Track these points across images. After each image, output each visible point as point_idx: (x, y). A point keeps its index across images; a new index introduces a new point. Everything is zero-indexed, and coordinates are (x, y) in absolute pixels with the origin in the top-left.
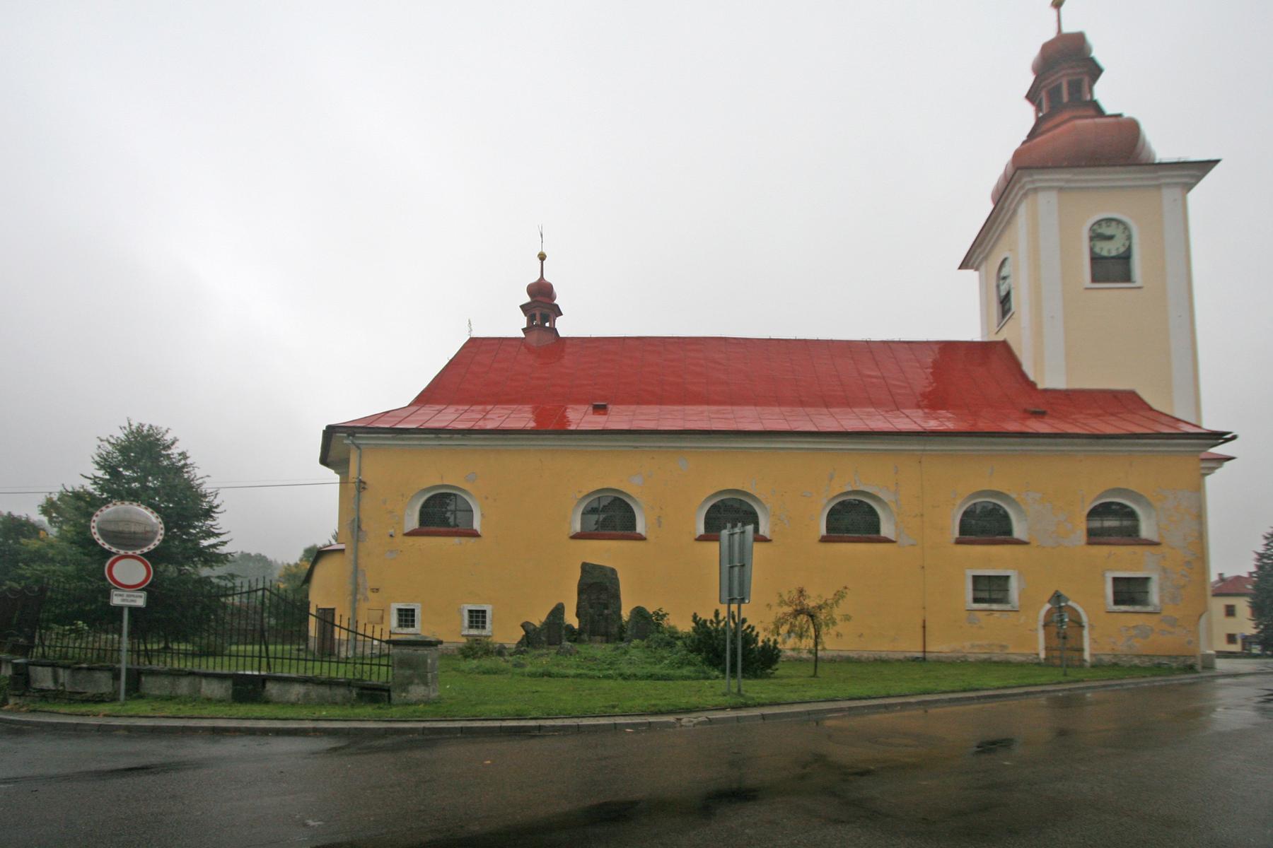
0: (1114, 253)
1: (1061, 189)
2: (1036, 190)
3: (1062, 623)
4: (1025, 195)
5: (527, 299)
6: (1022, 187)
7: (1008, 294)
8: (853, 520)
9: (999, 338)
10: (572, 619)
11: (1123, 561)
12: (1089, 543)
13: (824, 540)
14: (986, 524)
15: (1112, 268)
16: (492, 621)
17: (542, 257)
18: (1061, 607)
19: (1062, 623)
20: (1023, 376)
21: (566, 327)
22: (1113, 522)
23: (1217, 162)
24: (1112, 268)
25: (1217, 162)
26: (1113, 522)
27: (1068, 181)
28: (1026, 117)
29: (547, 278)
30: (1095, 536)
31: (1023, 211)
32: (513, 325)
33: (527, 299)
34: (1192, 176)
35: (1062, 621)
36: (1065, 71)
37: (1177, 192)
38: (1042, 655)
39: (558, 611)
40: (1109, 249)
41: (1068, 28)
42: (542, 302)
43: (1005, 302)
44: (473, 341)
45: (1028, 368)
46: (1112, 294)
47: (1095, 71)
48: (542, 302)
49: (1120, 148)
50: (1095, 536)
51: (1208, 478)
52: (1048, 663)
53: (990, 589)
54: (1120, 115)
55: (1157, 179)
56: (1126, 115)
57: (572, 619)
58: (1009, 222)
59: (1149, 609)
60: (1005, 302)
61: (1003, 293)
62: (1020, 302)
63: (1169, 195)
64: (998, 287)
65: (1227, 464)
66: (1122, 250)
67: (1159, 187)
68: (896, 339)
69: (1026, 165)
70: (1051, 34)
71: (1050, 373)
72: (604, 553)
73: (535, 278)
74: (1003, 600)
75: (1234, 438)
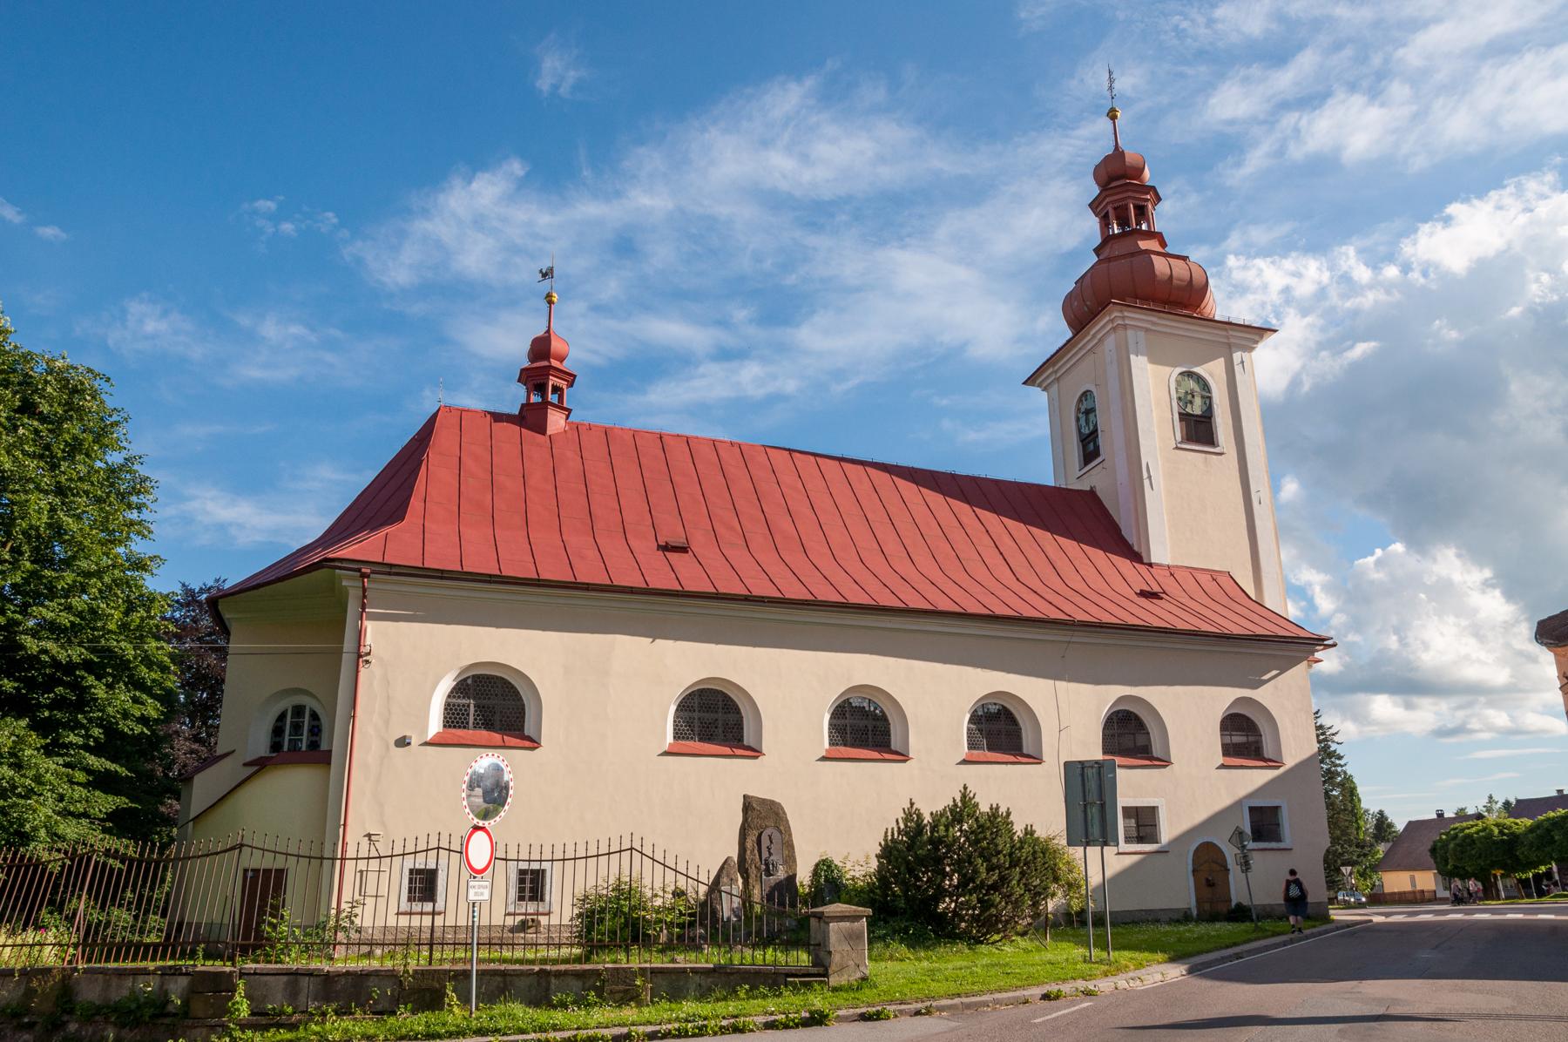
2: (1125, 327)
6: (1112, 321)
22: (1244, 737)
27: (1154, 323)
32: (514, 397)
46: (1194, 459)
59: (1281, 845)
61: (1086, 431)
75: (1334, 645)
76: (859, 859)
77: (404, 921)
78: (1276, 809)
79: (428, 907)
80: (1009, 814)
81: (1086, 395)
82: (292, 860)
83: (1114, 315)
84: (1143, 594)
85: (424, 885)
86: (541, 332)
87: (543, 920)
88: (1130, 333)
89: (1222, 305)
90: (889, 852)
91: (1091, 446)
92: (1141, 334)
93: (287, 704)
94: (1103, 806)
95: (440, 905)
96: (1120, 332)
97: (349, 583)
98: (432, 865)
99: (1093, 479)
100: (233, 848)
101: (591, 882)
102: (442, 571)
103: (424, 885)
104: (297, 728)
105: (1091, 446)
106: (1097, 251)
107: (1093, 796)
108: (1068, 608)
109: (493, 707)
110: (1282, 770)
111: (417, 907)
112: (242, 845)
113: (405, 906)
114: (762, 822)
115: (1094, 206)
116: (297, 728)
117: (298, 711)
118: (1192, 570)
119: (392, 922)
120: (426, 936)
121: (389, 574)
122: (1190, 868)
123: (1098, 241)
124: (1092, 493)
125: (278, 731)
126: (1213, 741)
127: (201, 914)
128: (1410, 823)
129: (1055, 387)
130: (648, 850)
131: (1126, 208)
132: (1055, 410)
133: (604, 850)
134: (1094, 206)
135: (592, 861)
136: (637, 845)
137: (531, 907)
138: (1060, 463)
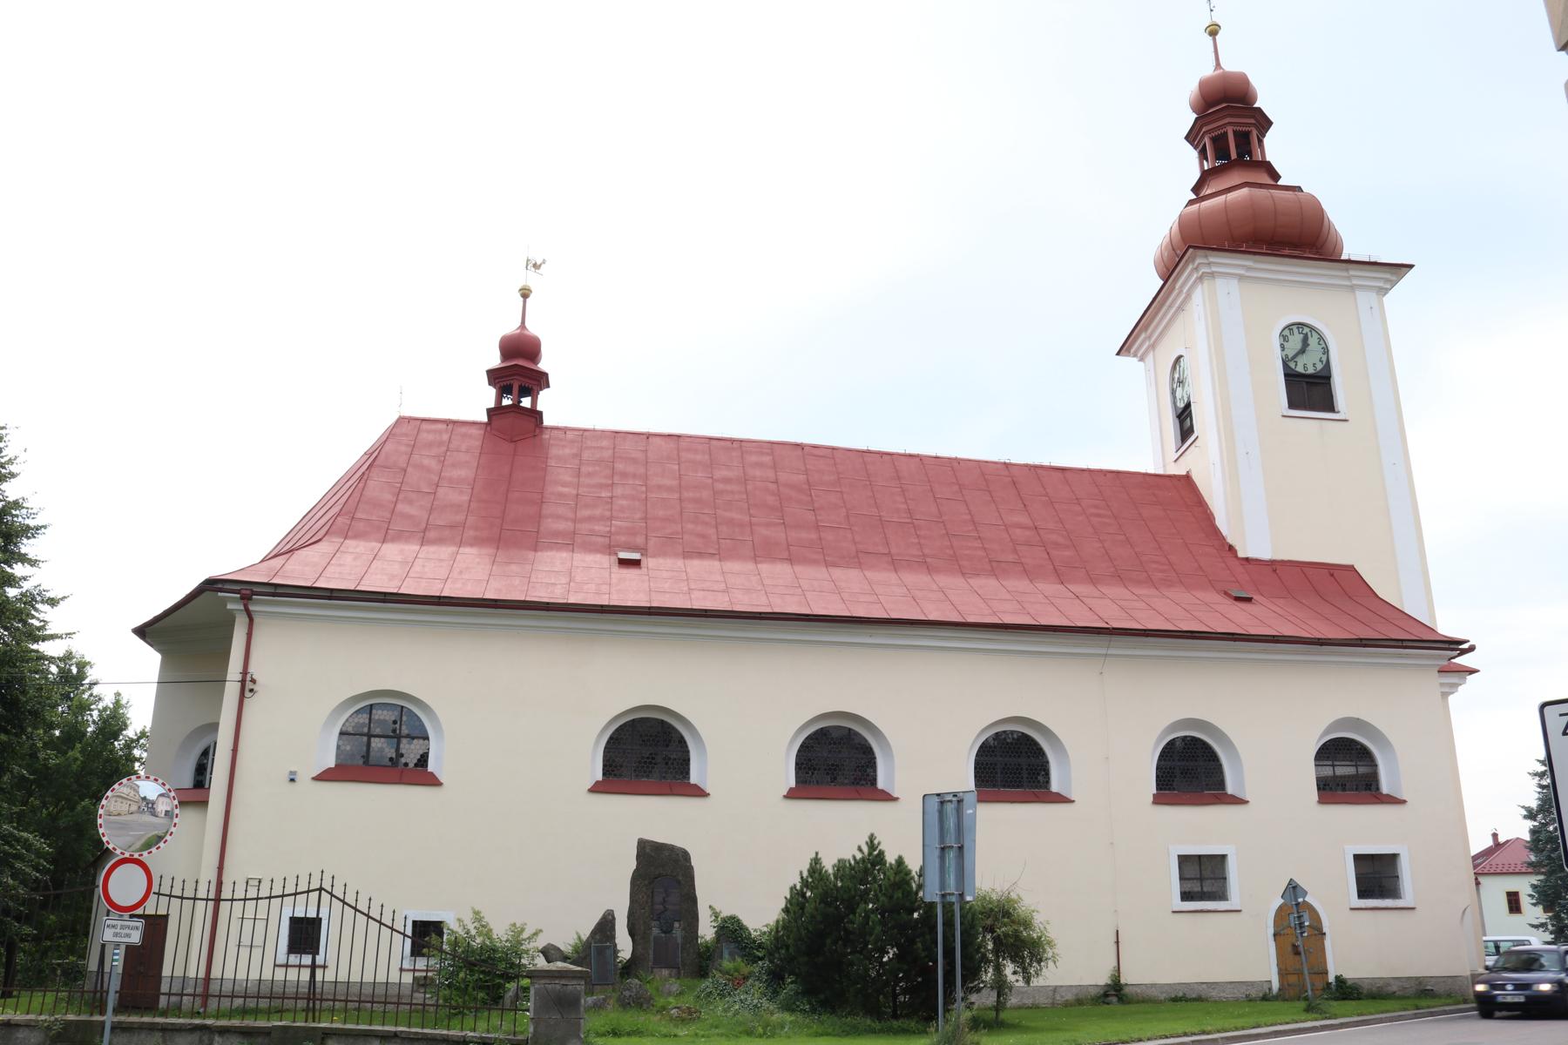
0: (1311, 371)
1: (1241, 278)
2: (1212, 275)
3: (1297, 927)
4: (1200, 279)
5: (495, 361)
6: (1196, 269)
7: (1188, 406)
9: (1179, 470)
10: (624, 945)
11: (1364, 828)
12: (1158, 800)
14: (1190, 770)
15: (1310, 390)
17: (1213, 31)
18: (1298, 904)
19: (1297, 927)
20: (1216, 532)
21: (554, 406)
22: (1348, 770)
23: (1411, 266)
24: (1310, 390)
25: (1411, 266)
26: (1348, 770)
27: (1249, 269)
28: (1189, 165)
29: (533, 329)
30: (1330, 790)
31: (1198, 296)
32: (475, 401)
34: (1387, 280)
35: (1301, 925)
36: (1228, 124)
37: (1373, 296)
38: (1276, 986)
39: (606, 926)
40: (1308, 364)
41: (1231, 65)
42: (519, 369)
43: (1184, 416)
45: (1221, 523)
46: (1309, 424)
47: (1264, 123)
48: (519, 369)
50: (1330, 790)
51: (1451, 698)
52: (1282, 996)
53: (1203, 878)
54: (1299, 189)
55: (1349, 278)
57: (624, 945)
58: (1180, 309)
60: (1184, 416)
61: (1181, 405)
62: (1203, 418)
63: (1365, 299)
64: (1173, 392)
65: (1470, 678)
66: (1320, 366)
67: (1352, 288)
68: (1046, 463)
69: (1198, 242)
70: (1208, 71)
71: (1255, 535)
72: (656, 817)
73: (510, 327)
74: (1221, 895)
75: (1472, 649)
76: (762, 913)
77: (280, 974)
78: (1393, 858)
79: (307, 960)
82: (176, 902)
84: (1249, 600)
85: (305, 935)
88: (1219, 282)
90: (796, 903)
92: (1235, 282)
94: (961, 848)
95: (320, 960)
102: (332, 590)
103: (305, 935)
107: (951, 841)
109: (383, 746)
111: (294, 959)
113: (282, 959)
119: (267, 975)
120: (304, 990)
121: (274, 595)
122: (1271, 931)
124: (1187, 478)
126: (1307, 775)
127: (356, 967)
128: (685, 855)
130: (338, 892)
133: (277, 891)
135: (188, 904)
136: (327, 886)
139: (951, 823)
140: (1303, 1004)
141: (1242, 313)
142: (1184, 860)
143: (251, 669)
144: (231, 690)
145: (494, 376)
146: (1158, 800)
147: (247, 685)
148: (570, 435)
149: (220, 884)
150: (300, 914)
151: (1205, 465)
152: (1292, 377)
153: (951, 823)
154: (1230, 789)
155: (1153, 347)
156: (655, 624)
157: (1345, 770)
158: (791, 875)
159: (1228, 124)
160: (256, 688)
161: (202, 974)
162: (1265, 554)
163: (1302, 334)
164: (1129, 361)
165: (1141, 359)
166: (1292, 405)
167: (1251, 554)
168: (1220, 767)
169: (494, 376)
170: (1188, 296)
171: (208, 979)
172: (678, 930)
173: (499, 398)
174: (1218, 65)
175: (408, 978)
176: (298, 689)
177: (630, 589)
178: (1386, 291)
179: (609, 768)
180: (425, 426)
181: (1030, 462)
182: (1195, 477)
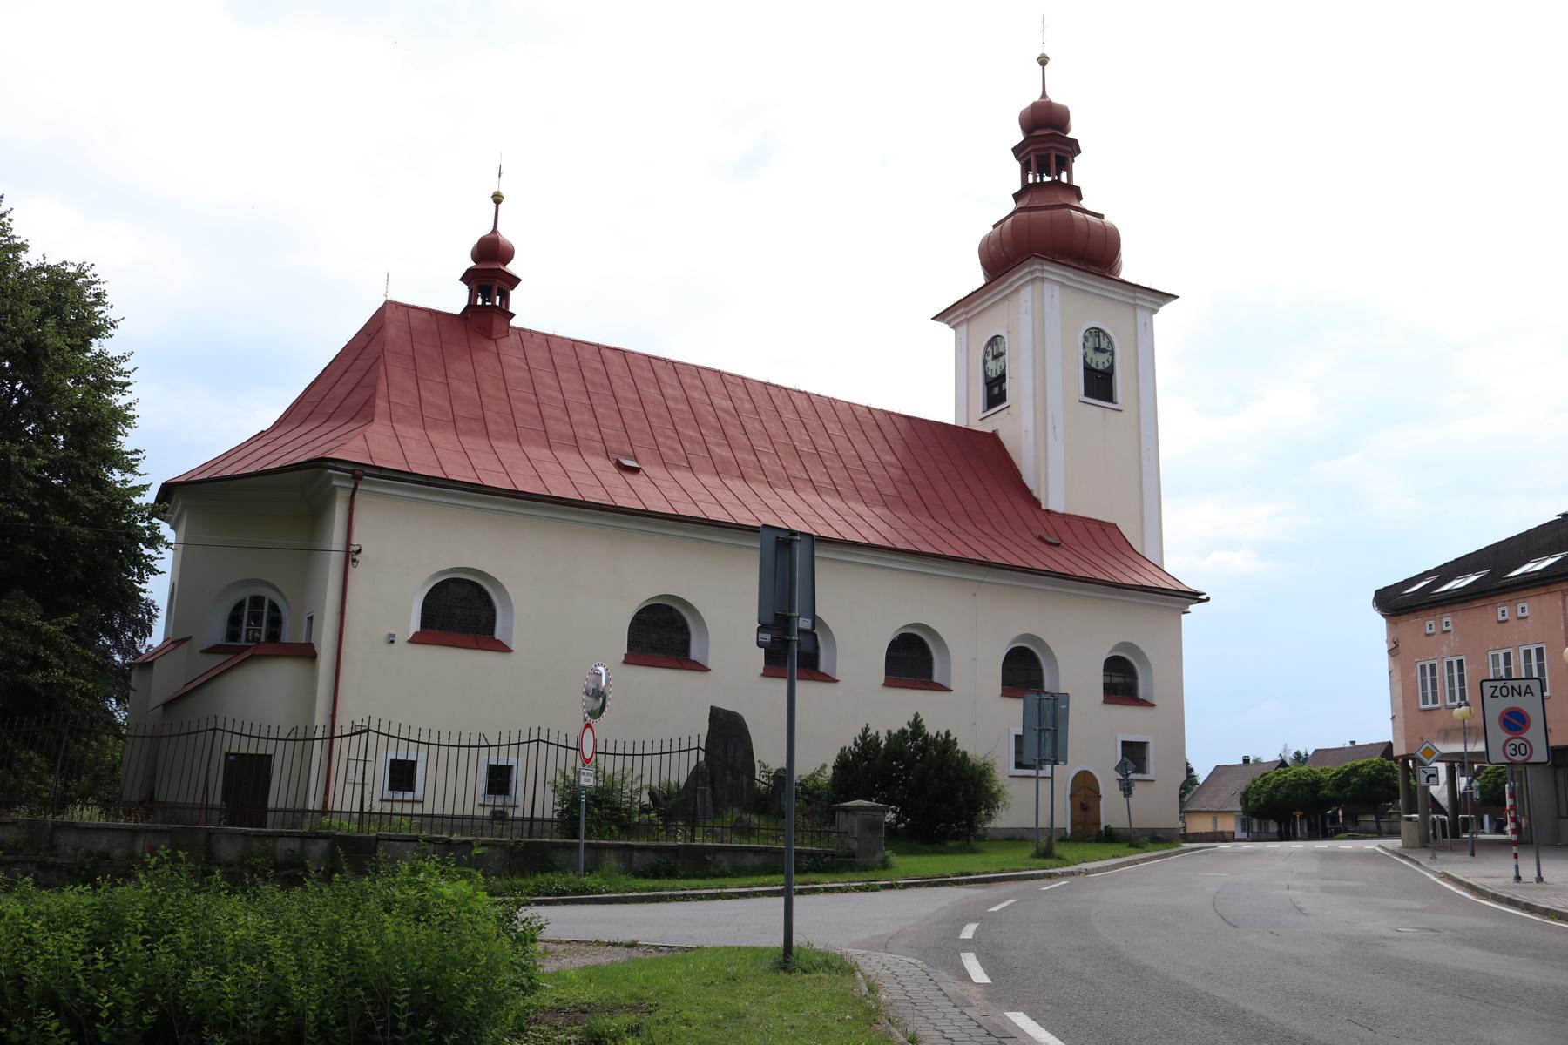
1: (1062, 285)
2: (1043, 280)
3: (1085, 790)
4: (1033, 281)
8: (460, 613)
11: (1128, 723)
12: (888, 684)
13: (416, 640)
15: (1099, 384)
16: (1324, 855)
17: (497, 199)
19: (1085, 790)
22: (1122, 680)
24: (1099, 384)
26: (1122, 680)
31: (1027, 294)
32: (455, 299)
33: (511, 268)
36: (1046, 139)
37: (1147, 314)
40: (1100, 362)
42: (491, 269)
44: (389, 306)
45: (1028, 478)
46: (1095, 411)
48: (491, 269)
49: (1092, 253)
56: (1109, 219)
59: (1146, 777)
75: (1208, 599)
80: (948, 734)
81: (994, 340)
83: (1038, 267)
85: (402, 775)
86: (486, 230)
87: (510, 812)
88: (1047, 285)
89: (1130, 270)
91: (996, 390)
92: (1057, 288)
93: (246, 594)
94: (1055, 731)
96: (1038, 285)
97: (341, 484)
98: (412, 757)
99: (997, 423)
100: (360, 733)
101: (665, 775)
103: (402, 775)
104: (256, 618)
105: (996, 390)
106: (1017, 197)
108: (981, 549)
109: (460, 613)
110: (162, 614)
111: (399, 795)
112: (215, 729)
114: (727, 731)
115: (1018, 151)
116: (256, 618)
117: (257, 601)
118: (766, 385)
123: (1018, 187)
125: (234, 619)
126: (1097, 680)
129: (964, 328)
131: (1048, 157)
132: (962, 350)
134: (1018, 151)
137: (499, 800)
138: (962, 400)
139: (1048, 713)
140: (1031, 849)
141: (1049, 311)
142: (1124, 743)
143: (355, 541)
144: (335, 562)
145: (468, 278)
146: (888, 684)
147: (350, 556)
148: (537, 340)
149: (333, 726)
150: (493, 762)
151: (1014, 428)
152: (1088, 370)
153: (1048, 713)
154: (936, 679)
155: (968, 320)
156: (521, 506)
157: (1117, 679)
158: (847, 739)
159: (1046, 139)
160: (357, 557)
161: (356, 808)
162: (1061, 510)
163: (1097, 339)
164: (945, 332)
165: (953, 327)
166: (1087, 394)
167: (1051, 507)
168: (1041, 670)
169: (468, 278)
170: (1017, 290)
171: (361, 812)
172: (744, 780)
173: (472, 298)
174: (1044, 95)
175: (488, 812)
176: (388, 562)
177: (622, 493)
178: (1155, 311)
179: (889, 670)
180: (412, 312)
181: (890, 409)
182: (1002, 436)
